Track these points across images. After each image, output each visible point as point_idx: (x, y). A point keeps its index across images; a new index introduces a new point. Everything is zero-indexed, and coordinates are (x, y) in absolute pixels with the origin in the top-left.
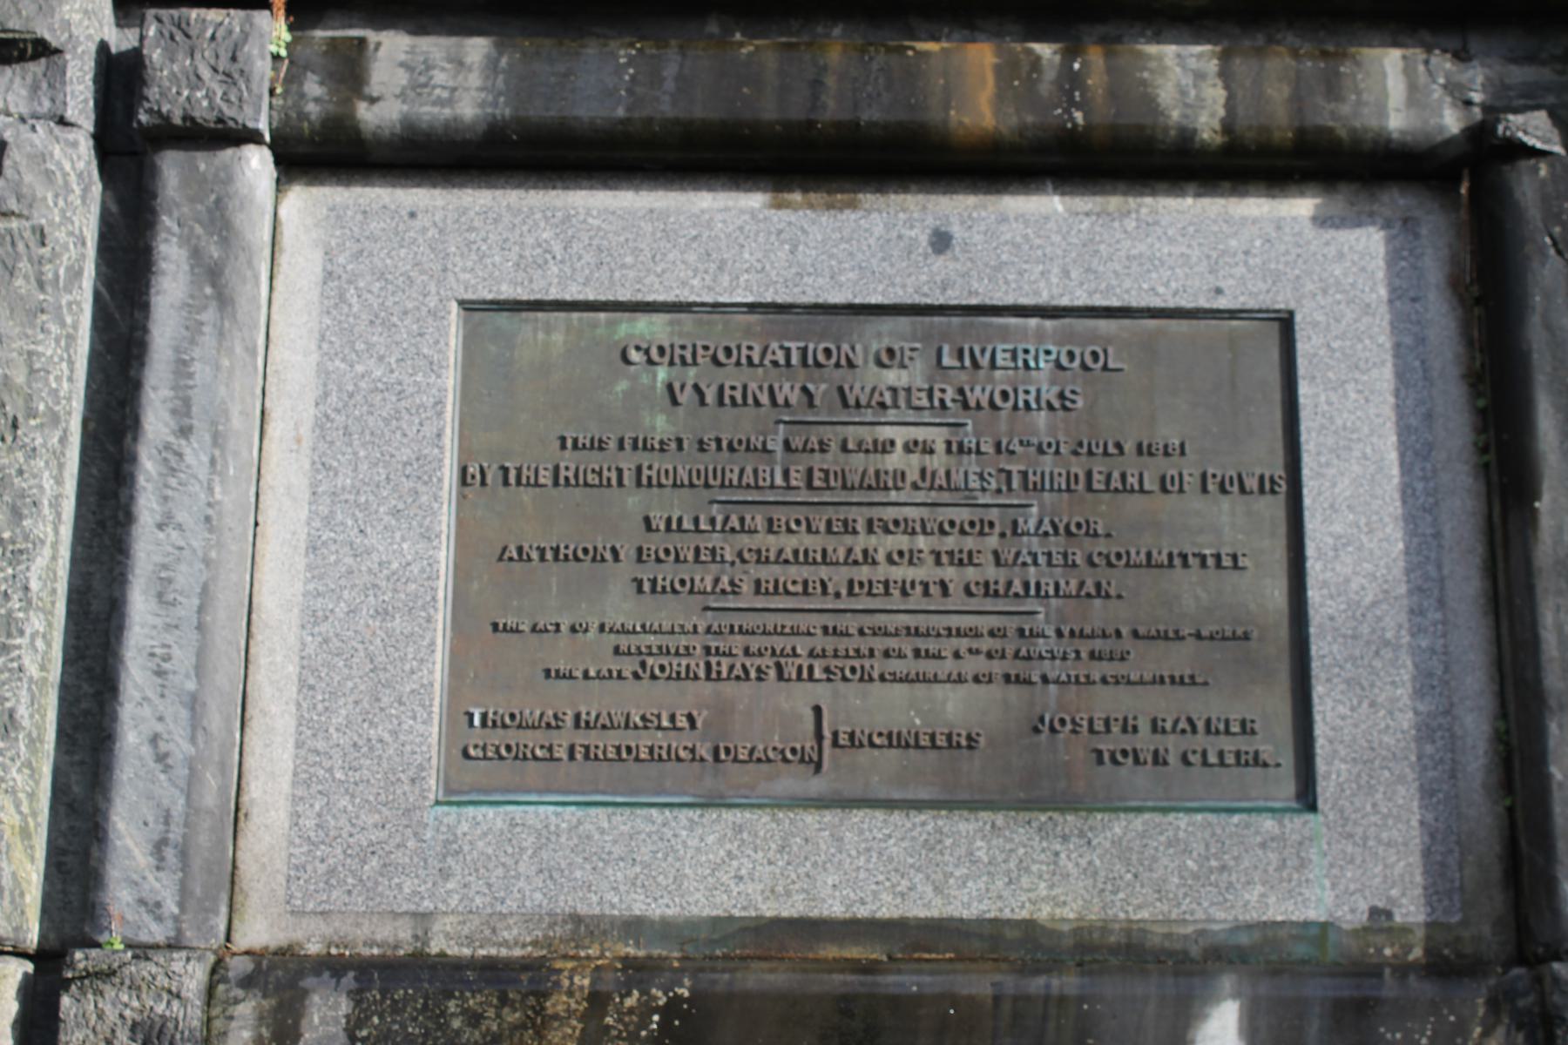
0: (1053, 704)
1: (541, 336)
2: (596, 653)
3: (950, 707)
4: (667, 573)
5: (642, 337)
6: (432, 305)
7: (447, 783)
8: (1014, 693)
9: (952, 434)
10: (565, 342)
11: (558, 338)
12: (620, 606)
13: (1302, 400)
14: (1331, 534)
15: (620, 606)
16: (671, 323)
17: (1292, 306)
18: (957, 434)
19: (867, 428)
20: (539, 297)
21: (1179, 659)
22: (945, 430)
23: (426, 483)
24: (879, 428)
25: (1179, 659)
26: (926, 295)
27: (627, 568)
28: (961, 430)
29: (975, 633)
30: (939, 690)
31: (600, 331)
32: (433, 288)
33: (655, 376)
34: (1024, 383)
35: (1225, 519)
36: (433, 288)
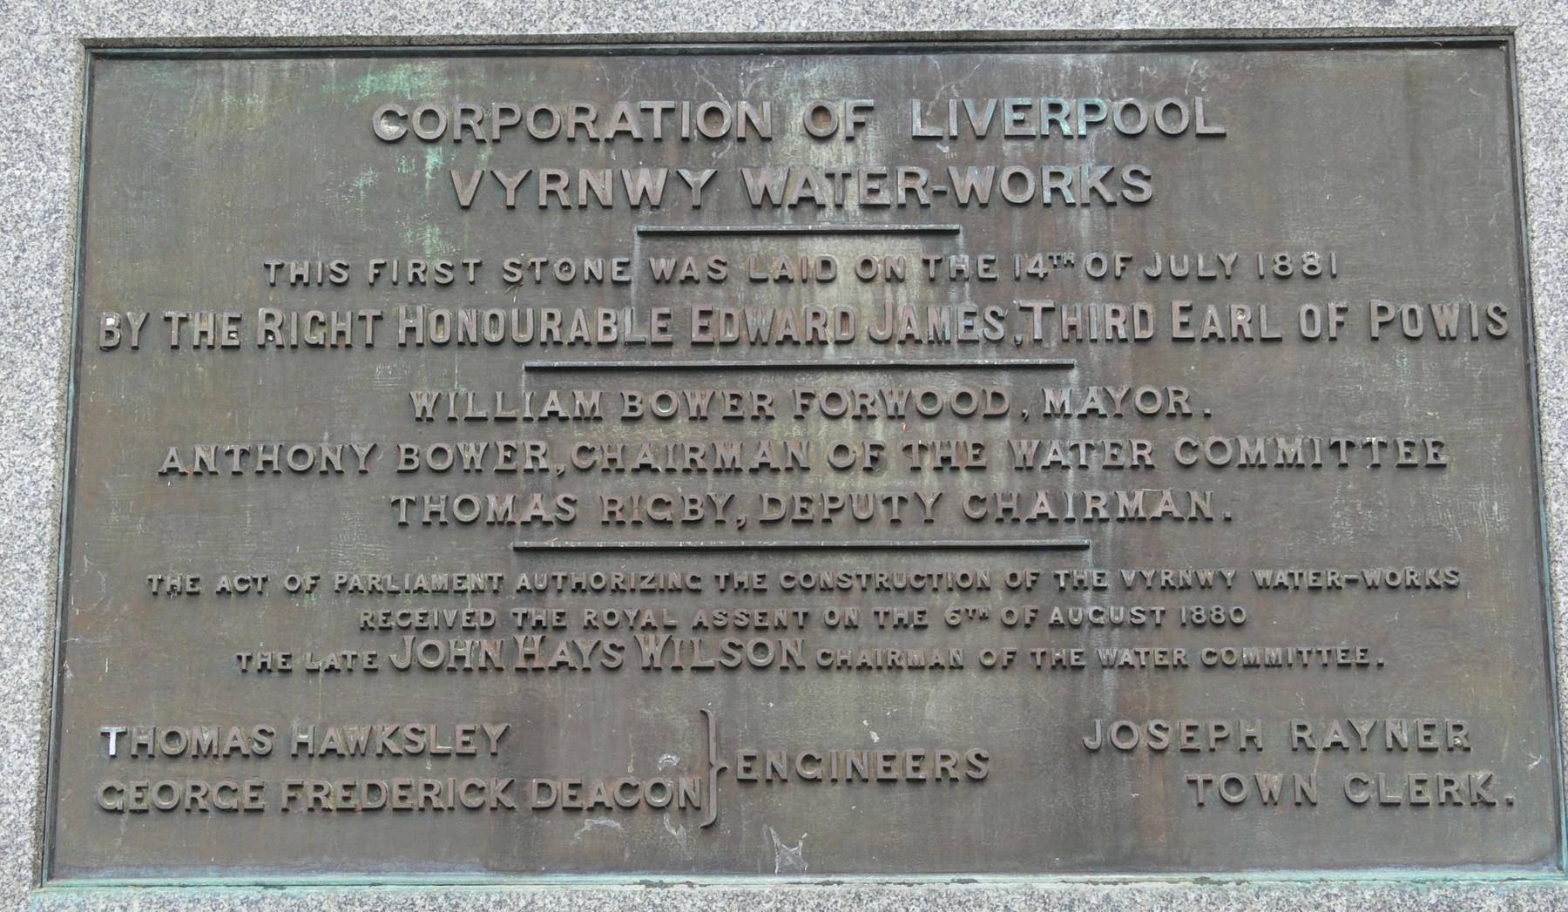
0: (1108, 702)
1: (227, 98)
2: (326, 635)
3: (930, 711)
4: (436, 496)
5: (399, 97)
6: (42, 48)
7: (1510, 60)
8: (1046, 690)
9: (930, 251)
10: (270, 107)
11: (257, 101)
12: (361, 549)
13: (1532, 179)
14: (1198, 508)
15: (361, 549)
16: (449, 74)
17: (1514, 20)
18: (937, 250)
19: (784, 243)
20: (223, 32)
21: (1334, 624)
22: (916, 244)
23: (29, 346)
24: (804, 243)
25: (1334, 624)
26: (885, 18)
27: (382, 482)
28: (945, 243)
29: (966, 586)
30: (910, 685)
31: (331, 88)
32: (42, 21)
33: (422, 161)
34: (1051, 161)
35: (1404, 383)
36: (42, 21)
